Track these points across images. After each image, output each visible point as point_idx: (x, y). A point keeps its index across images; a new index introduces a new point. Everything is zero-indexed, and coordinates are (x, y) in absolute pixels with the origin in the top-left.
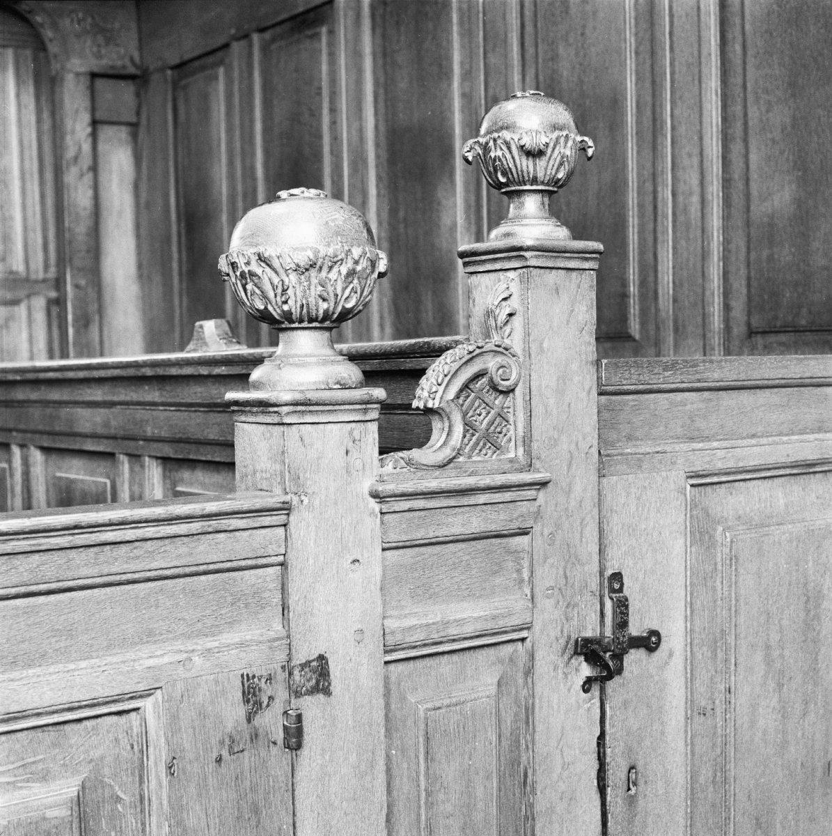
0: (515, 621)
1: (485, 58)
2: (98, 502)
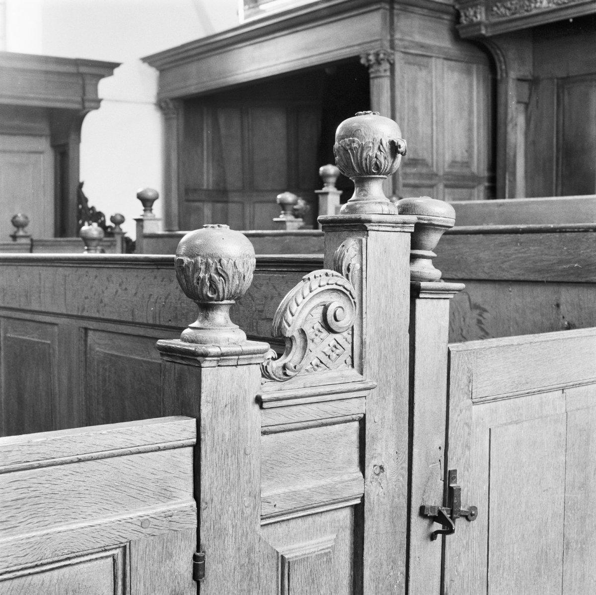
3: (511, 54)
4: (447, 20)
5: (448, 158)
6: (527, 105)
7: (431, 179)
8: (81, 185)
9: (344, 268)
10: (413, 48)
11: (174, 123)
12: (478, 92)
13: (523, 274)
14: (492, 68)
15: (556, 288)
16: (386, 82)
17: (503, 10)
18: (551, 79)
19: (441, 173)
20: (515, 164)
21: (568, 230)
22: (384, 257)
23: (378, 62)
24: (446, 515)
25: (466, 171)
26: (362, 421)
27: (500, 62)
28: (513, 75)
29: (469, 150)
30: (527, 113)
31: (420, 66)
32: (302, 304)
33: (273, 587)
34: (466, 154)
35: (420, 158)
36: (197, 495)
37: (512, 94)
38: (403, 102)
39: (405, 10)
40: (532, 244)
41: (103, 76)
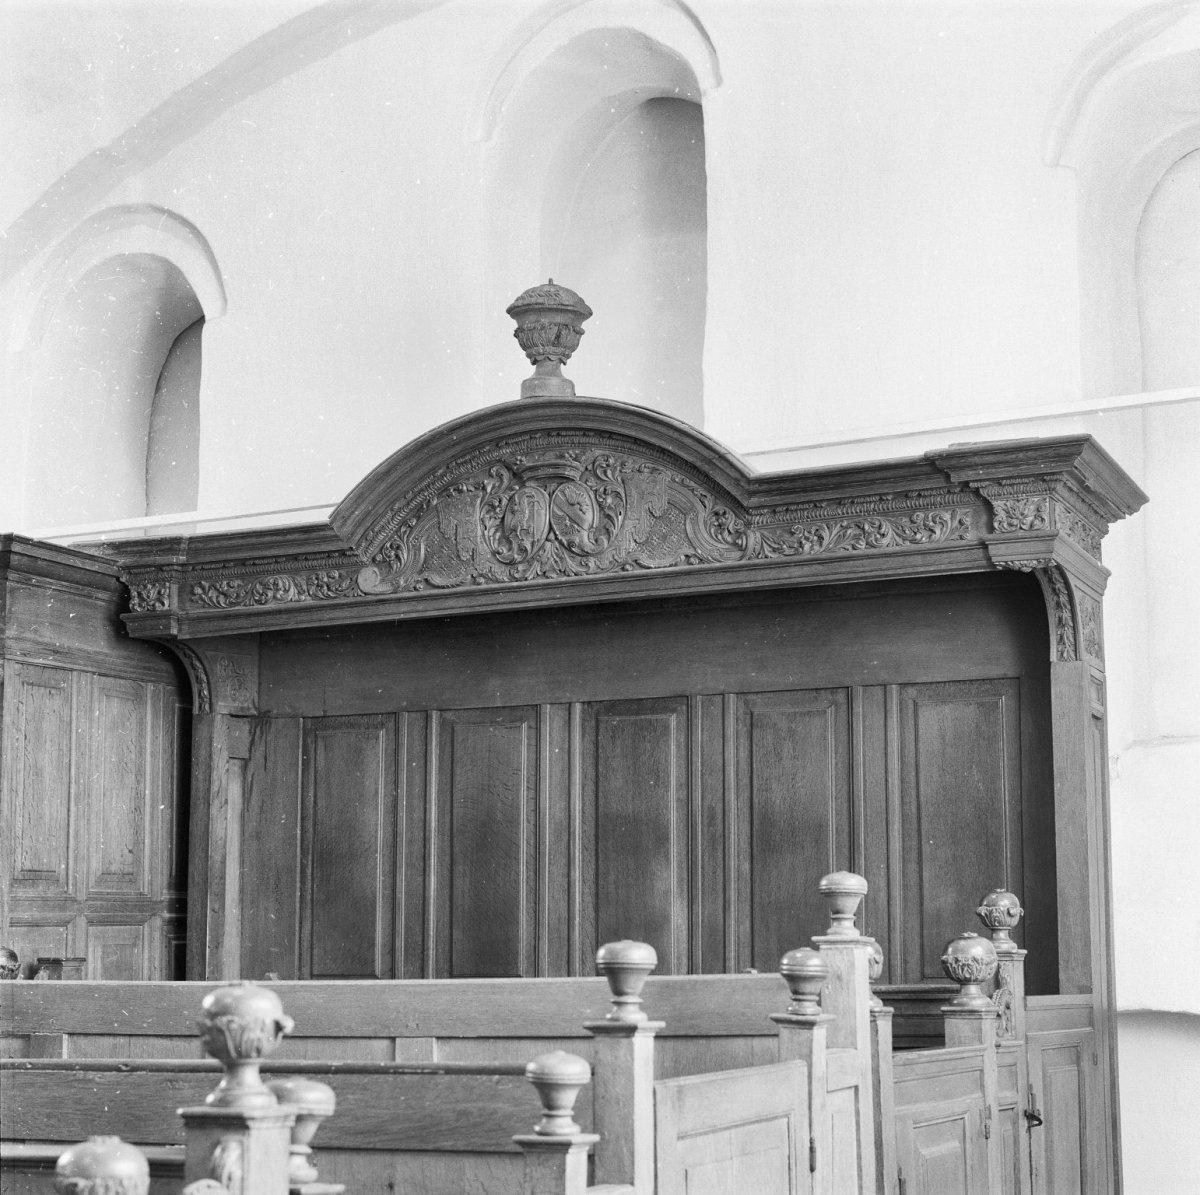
0: (1010, 1101)
1: (702, 778)
2: (772, 1062)
3: (219, 670)
4: (104, 600)
5: (96, 865)
6: (245, 763)
7: (63, 909)
9: (225, 1178)
10: (38, 654)
12: (155, 738)
13: (336, 1138)
14: (184, 691)
15: (387, 1158)
17: (212, 594)
18: (294, 717)
19: (82, 896)
20: (223, 877)
21: (406, 1070)
25: (129, 891)
27: (199, 680)
28: (223, 707)
29: (135, 850)
30: (244, 778)
31: (53, 688)
33: (857, 1193)
34: (129, 858)
35: (45, 868)
37: (221, 742)
38: (15, 759)
39: (27, 582)
40: (350, 1091)
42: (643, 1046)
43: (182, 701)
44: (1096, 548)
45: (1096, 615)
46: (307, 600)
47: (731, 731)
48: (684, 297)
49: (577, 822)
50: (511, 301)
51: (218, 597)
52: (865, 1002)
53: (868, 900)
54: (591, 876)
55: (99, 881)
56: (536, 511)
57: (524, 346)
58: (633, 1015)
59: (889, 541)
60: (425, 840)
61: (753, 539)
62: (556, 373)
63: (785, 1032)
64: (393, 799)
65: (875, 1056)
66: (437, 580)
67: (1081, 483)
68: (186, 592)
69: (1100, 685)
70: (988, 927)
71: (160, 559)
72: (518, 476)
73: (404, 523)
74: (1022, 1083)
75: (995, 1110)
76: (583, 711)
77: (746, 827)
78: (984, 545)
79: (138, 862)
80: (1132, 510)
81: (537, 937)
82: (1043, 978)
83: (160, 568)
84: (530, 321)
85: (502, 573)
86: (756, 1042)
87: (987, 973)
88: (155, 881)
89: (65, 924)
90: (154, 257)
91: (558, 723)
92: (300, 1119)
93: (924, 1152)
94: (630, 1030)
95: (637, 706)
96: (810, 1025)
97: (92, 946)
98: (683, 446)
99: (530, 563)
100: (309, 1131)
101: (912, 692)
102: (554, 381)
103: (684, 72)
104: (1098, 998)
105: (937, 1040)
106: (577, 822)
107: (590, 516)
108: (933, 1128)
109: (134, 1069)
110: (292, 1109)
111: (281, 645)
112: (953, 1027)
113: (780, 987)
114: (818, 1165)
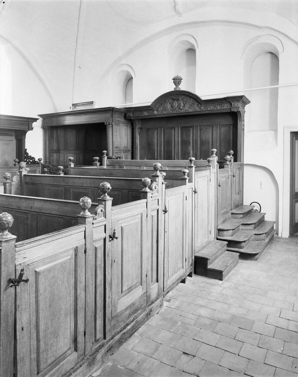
8: (26, 149)
11: (48, 132)
16: (111, 129)
22: (160, 180)
23: (109, 124)
24: (165, 211)
26: (158, 199)
28: (137, 127)
32: (154, 185)
36: (147, 208)
41: (34, 122)
42: (194, 168)
43: (132, 126)
44: (244, 108)
45: (244, 117)
46: (148, 115)
47: (198, 130)
48: (193, 76)
49: (180, 141)
50: (173, 78)
51: (137, 114)
52: (216, 163)
53: (217, 152)
54: (181, 147)
55: (124, 148)
56: (176, 104)
57: (174, 84)
58: (192, 165)
59: (219, 108)
60: (161, 143)
61: (202, 108)
62: (178, 87)
63: (207, 167)
64: (158, 138)
65: (217, 169)
66: (163, 112)
67: (243, 101)
68: (133, 114)
69: (244, 125)
70: (229, 155)
71: (130, 110)
72: (173, 100)
73: (159, 105)
74: (233, 172)
75: (230, 175)
76: (180, 128)
77: (200, 142)
78: (230, 109)
79: (128, 145)
80: (249, 103)
81: (175, 154)
82: (235, 160)
83: (130, 111)
84: (175, 80)
85: (171, 112)
86: (204, 168)
87: (229, 160)
88: (130, 147)
89: (120, 153)
90: (127, 71)
91: (177, 129)
92: (163, 176)
93: (222, 180)
94: (192, 167)
95: (187, 127)
96: (210, 166)
97: (123, 155)
98: (194, 96)
99: (175, 110)
100: (164, 177)
101: (220, 126)
102: (178, 88)
103: (193, 45)
104: (242, 163)
105: (223, 167)
106: (180, 141)
107: (182, 105)
108: (223, 177)
109: (138, 170)
110: (162, 175)
111: (144, 120)
112: (225, 166)
113: (207, 162)
114: (211, 181)
